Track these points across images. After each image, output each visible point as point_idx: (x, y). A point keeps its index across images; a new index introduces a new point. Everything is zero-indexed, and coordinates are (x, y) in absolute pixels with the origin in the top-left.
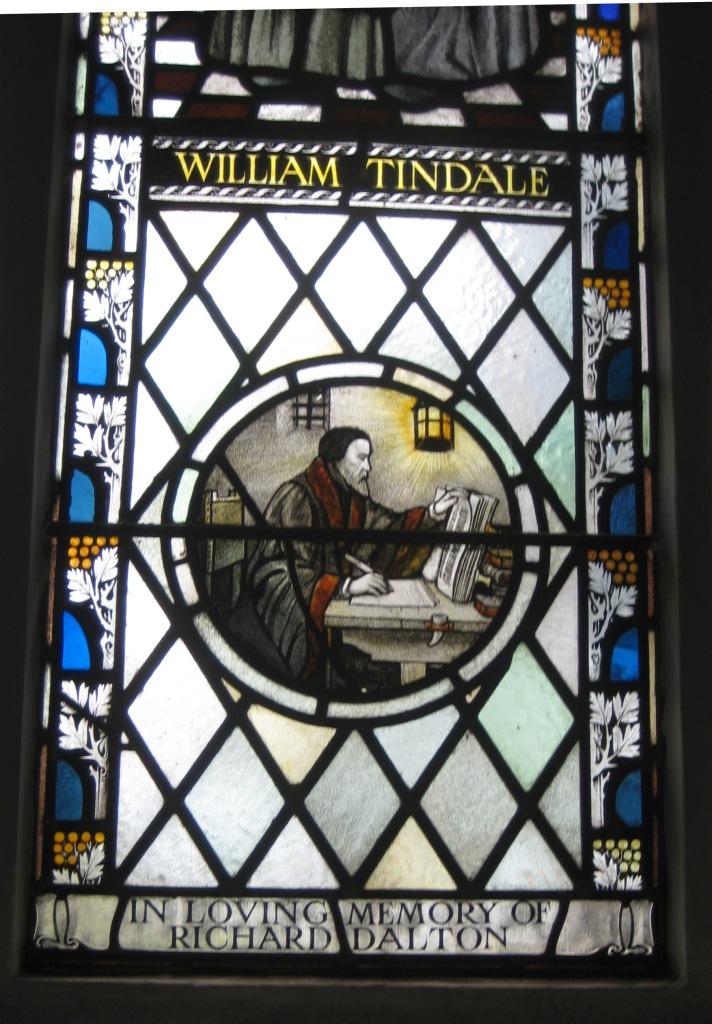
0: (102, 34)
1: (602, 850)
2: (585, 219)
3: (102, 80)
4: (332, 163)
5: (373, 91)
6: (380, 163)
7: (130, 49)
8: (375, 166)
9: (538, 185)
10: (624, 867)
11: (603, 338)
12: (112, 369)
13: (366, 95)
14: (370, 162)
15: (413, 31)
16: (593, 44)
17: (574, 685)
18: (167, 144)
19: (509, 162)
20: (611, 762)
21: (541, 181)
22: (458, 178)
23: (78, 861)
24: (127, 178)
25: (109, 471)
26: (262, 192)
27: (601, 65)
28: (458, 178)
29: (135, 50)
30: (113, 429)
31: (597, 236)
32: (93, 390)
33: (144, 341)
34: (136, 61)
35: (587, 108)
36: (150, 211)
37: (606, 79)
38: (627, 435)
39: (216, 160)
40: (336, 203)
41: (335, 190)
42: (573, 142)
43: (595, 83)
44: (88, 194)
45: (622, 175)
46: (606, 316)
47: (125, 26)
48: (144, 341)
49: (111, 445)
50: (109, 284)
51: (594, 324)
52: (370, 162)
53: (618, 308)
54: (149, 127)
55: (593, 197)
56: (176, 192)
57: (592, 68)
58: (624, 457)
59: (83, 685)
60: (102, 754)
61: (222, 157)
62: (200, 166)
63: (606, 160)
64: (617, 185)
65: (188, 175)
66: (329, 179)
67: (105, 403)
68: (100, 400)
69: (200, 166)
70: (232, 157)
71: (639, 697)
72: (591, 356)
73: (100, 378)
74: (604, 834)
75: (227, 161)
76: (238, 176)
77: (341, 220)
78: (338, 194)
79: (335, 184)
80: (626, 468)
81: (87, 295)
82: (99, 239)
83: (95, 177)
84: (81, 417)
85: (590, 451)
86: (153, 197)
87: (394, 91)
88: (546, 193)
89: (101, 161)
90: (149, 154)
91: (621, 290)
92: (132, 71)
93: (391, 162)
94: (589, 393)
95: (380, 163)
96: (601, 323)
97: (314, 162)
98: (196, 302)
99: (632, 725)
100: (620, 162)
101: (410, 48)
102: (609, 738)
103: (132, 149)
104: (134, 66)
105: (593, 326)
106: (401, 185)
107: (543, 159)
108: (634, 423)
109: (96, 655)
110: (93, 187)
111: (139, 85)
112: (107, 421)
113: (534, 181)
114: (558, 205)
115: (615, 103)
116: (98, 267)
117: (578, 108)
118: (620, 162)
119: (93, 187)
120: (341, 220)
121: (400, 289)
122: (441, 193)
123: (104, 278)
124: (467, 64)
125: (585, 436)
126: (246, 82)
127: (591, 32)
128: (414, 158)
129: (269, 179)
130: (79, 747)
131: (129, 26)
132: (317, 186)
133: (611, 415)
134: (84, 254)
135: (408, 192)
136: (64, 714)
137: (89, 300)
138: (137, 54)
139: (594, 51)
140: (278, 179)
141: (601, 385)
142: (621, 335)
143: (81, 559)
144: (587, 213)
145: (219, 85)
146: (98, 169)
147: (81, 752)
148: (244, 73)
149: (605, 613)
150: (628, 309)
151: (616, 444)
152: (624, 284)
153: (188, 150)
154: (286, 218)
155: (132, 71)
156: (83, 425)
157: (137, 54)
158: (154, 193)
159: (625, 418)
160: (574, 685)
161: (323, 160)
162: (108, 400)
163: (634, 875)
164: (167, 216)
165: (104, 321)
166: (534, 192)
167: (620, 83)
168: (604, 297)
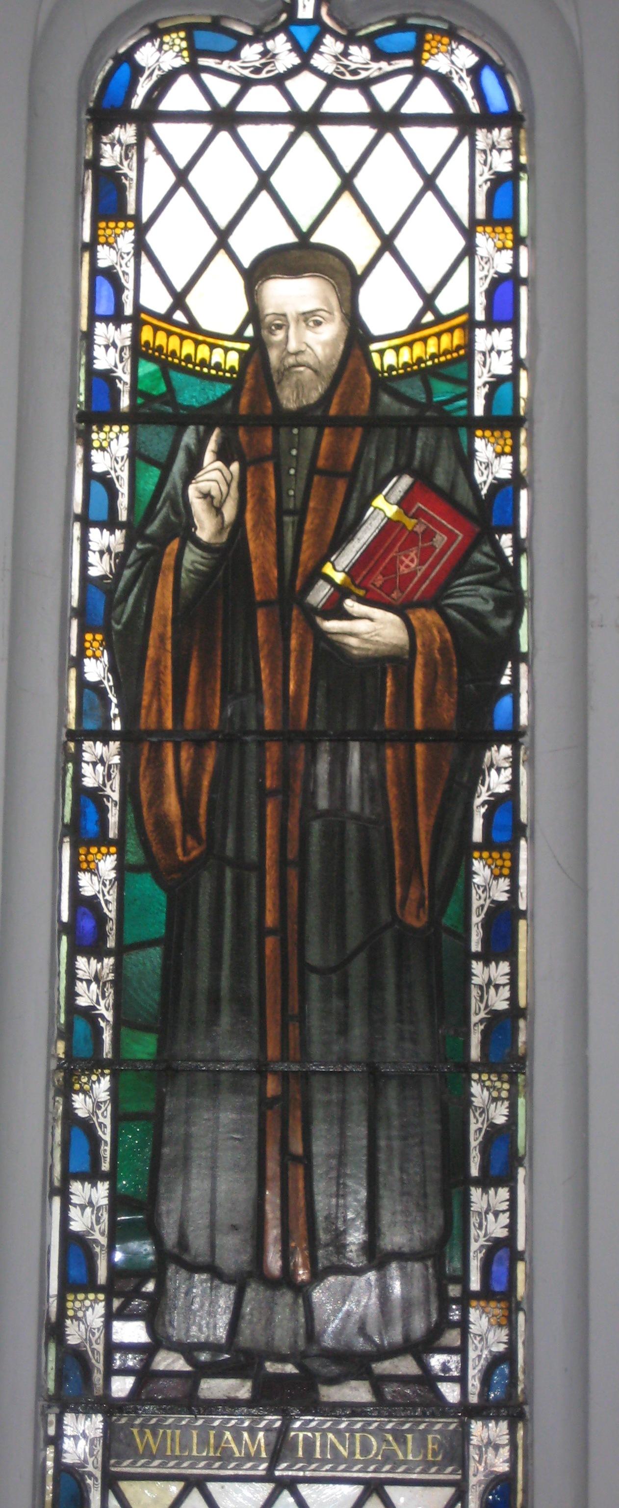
0: (93, 448)
1: (480, 1081)
2: (473, 1480)
3: (84, 799)
4: (261, 1435)
5: (297, 1365)
6: (301, 1435)
7: (91, 1331)
8: (297, 1436)
9: (433, 1449)
10: (495, 1094)
11: (488, 901)
12: (96, 1159)
13: (290, 1368)
14: (292, 1434)
15: (329, 1307)
16: (484, 1316)
17: (466, 222)
18: (123, 1421)
19: (409, 1431)
20: (487, 1014)
21: (436, 1447)
22: (366, 1449)
23: (85, 1315)
24: (98, 1221)
25: (126, 176)
26: (202, 1464)
27: (491, 1335)
28: (366, 1449)
29: (96, 1331)
30: (99, 1208)
31: (484, 1033)
32: (106, 319)
33: (143, 254)
34: (96, 1341)
35: (480, 925)
36: (111, 1482)
37: (495, 1349)
38: (505, 1206)
39: (165, 1433)
40: (263, 1473)
41: (262, 1460)
42: (468, 1412)
43: (486, 1352)
44: (95, 271)
45: (505, 1439)
46: (488, 1330)
47: (112, 440)
48: (143, 254)
49: (121, 361)
50: (84, 1312)
51: (484, 466)
52: (292, 1434)
53: (501, 875)
54: (109, 1407)
55: (484, 365)
56: (133, 1464)
57: (485, 887)
58: (503, 998)
59: (92, 959)
60: (107, 1009)
61: (169, 1431)
62: (151, 1441)
63: (492, 1191)
64: (503, 770)
65: (141, 1448)
66: (258, 1451)
67: (92, 1187)
68: (87, 1186)
69: (151, 1441)
70: (178, 1432)
71: (507, 791)
72: (478, 916)
73: (86, 1167)
74: (483, 223)
75: (173, 1434)
76: (182, 1449)
77: (266, 1489)
78: (264, 1466)
79: (264, 1455)
80: (507, 168)
81: (93, 452)
82: (105, 307)
83: (96, 358)
84: (75, 1199)
85: (479, 158)
86: (113, 1469)
87: (316, 1365)
88: (439, 1458)
89: (94, 552)
90: (109, 1429)
91: (504, 860)
92: (118, 478)
93: (310, 1434)
94: (480, 315)
95: (301, 1435)
96: (484, 1111)
97: (246, 1435)
98: (179, 287)
99: (504, 985)
100: (504, 1425)
101: (327, 1323)
102: (484, 1223)
103: (94, 1425)
104: (95, 1346)
105: (480, 892)
106: (318, 1456)
107: (438, 1427)
108: (510, 1196)
109: (119, 305)
110: (95, 366)
111: (98, 1364)
112: (122, 141)
113: (430, 1446)
114: (450, 1469)
115: (506, 389)
116: (94, 639)
117: (470, 1377)
118: (504, 1425)
119: (95, 366)
120: (266, 1489)
121: (336, 181)
122: (351, 1462)
123: (105, 440)
124: (377, 1340)
125: (469, 1440)
126: (190, 1360)
127: (489, 229)
128: (329, 1429)
129: (208, 1453)
130: (108, 367)
131: (115, 440)
132: (248, 1458)
133: (493, 963)
134: (93, 318)
135: (323, 1461)
136: (85, 762)
137: (96, 455)
138: (97, 1335)
139: (485, 1320)
140: (215, 1452)
141: (489, 309)
142: (501, 1120)
143: (88, 862)
144: (475, 1475)
145: (169, 1361)
146: (68, 1444)
147: (116, 168)
148: (188, 1350)
149: (485, 900)
150: (510, 454)
151: (497, 987)
152: (507, 855)
153: (142, 1426)
154: (223, 1487)
155: (93, 1350)
156: (88, 763)
157: (97, 1335)
158: (114, 1466)
159: (507, 333)
160: (465, 221)
161: (252, 1431)
162: (118, 326)
163: (503, 1100)
164: (124, 1485)
165: (108, 473)
166: (430, 1458)
167: (507, 794)
168: (489, 867)
